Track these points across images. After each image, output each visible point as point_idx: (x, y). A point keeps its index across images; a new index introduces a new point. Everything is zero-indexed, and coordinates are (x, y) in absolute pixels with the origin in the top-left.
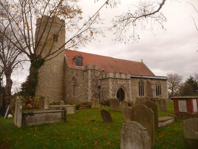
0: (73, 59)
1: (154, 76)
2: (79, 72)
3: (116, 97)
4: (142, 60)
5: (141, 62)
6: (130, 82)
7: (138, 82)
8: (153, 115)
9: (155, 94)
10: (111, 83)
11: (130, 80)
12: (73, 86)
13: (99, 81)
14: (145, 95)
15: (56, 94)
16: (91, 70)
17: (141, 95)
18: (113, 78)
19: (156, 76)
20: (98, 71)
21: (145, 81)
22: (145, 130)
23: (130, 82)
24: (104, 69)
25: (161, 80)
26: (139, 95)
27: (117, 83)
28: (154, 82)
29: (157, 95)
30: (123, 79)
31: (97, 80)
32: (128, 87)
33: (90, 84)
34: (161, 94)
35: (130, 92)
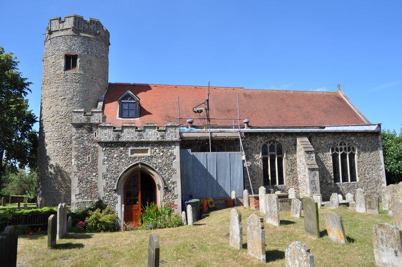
34: (353, 178)
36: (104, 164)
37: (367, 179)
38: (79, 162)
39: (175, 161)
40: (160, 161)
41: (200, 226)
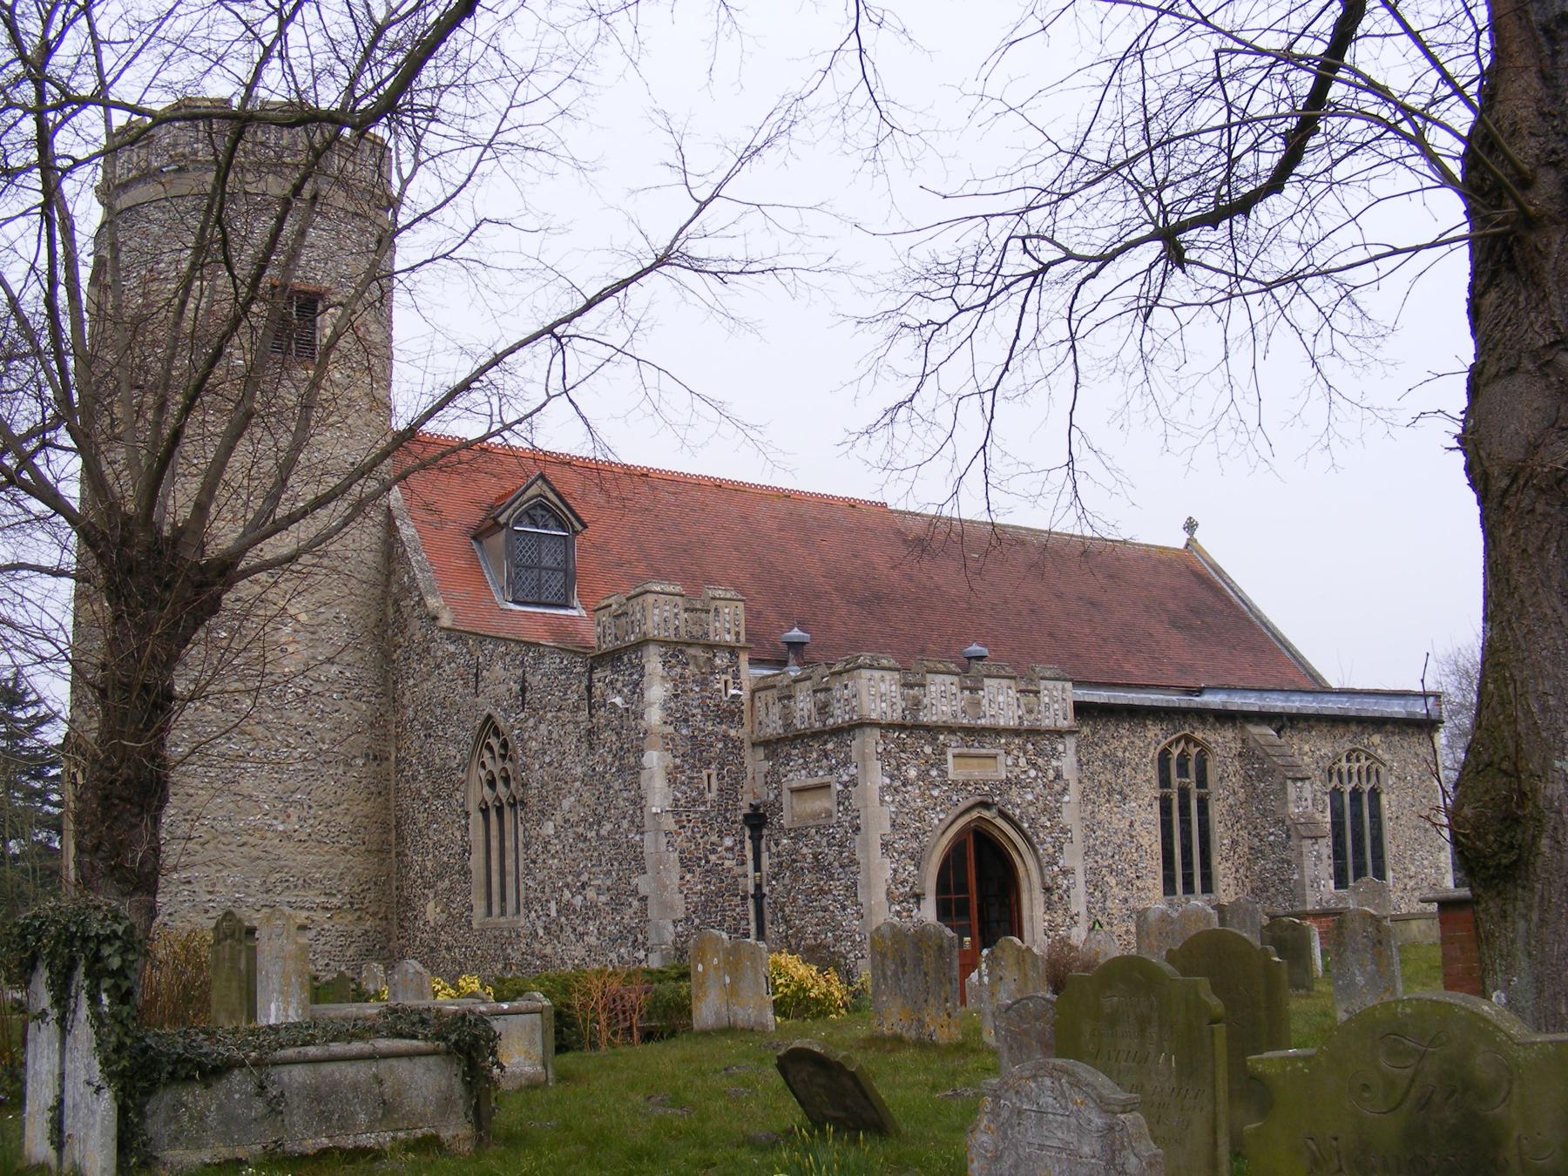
0: (479, 535)
1: (1320, 688)
2: (550, 663)
3: (928, 912)
4: (1191, 526)
5: (1178, 540)
6: (1067, 760)
7: (1153, 753)
8: (1221, 1029)
9: (1326, 869)
10: (876, 778)
11: (1071, 742)
12: (485, 812)
13: (756, 763)
14: (1227, 888)
15: (313, 897)
16: (675, 649)
17: (1188, 888)
18: (902, 727)
19: (1335, 685)
20: (744, 658)
21: (1221, 741)
22: (1126, 1108)
23: (1067, 760)
24: (796, 634)
25: (1379, 723)
26: (1169, 888)
27: (944, 773)
28: (1310, 750)
29: (1341, 881)
30: (997, 732)
31: (735, 746)
32: (1053, 812)
33: (659, 796)
34: (1380, 873)
35: (1072, 857)
36: (882, 802)
37: (1411, 877)
38: (679, 795)
39: (1066, 798)
40: (1030, 797)
41: (69, 1101)
